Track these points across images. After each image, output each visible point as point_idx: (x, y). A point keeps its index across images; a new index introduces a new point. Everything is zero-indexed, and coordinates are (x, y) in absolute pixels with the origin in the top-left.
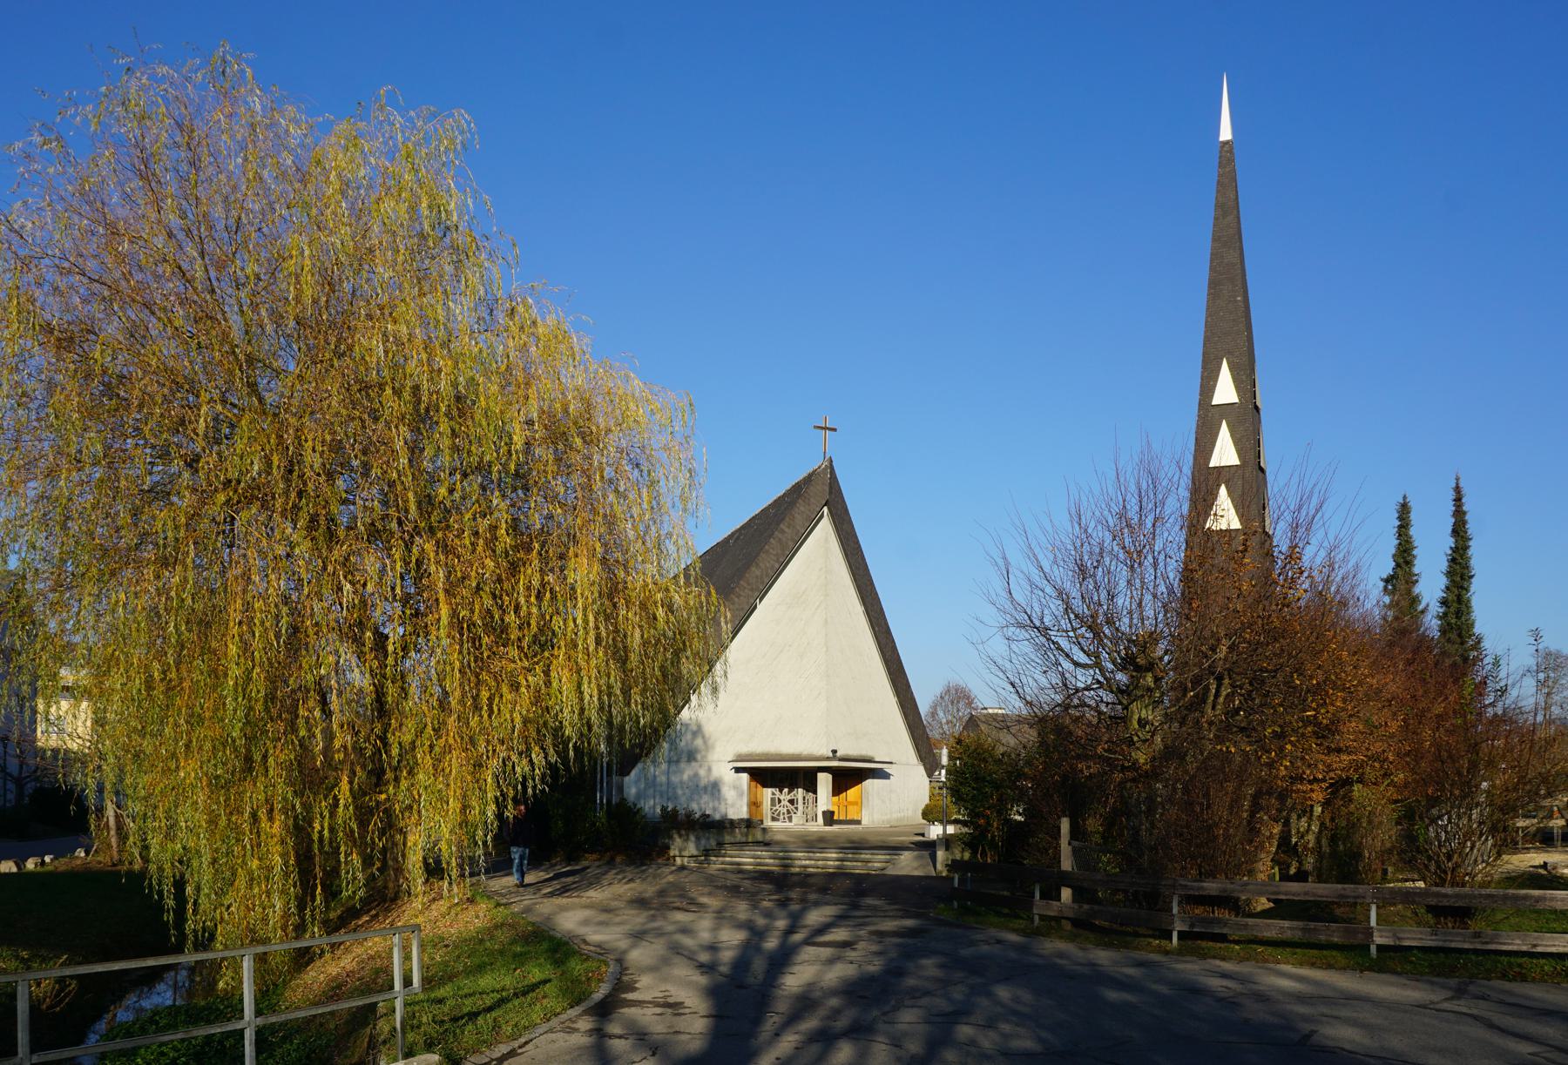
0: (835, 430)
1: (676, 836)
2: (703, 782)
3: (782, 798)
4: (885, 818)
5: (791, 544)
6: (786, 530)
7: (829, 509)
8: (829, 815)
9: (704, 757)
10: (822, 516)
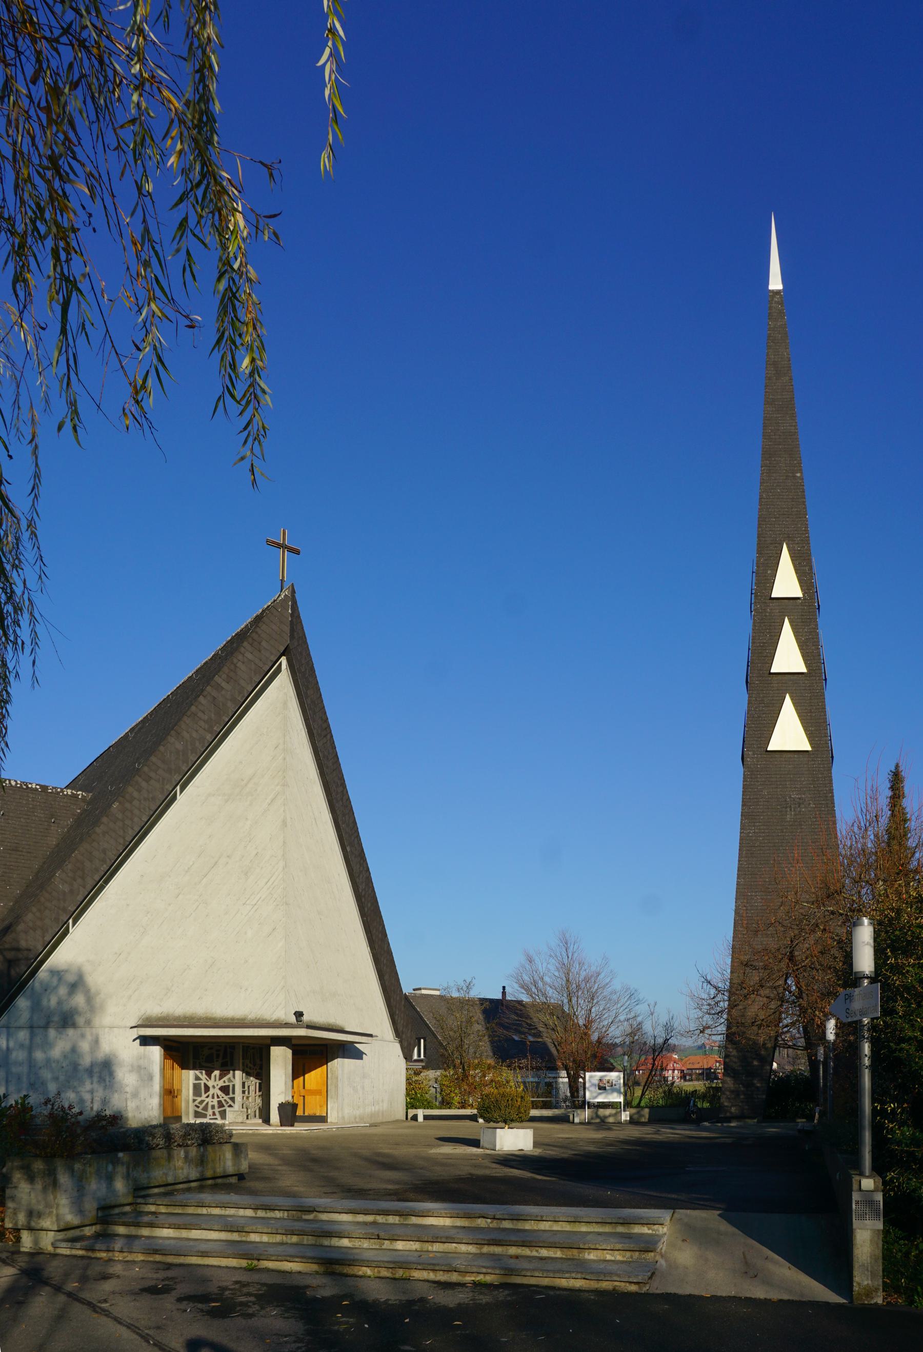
0: (297, 552)
1: (17, 1176)
2: (86, 1061)
3: (210, 1084)
4: (358, 1113)
5: (231, 707)
6: (224, 684)
7: (288, 661)
8: (290, 1108)
9: (88, 1023)
10: (279, 670)
